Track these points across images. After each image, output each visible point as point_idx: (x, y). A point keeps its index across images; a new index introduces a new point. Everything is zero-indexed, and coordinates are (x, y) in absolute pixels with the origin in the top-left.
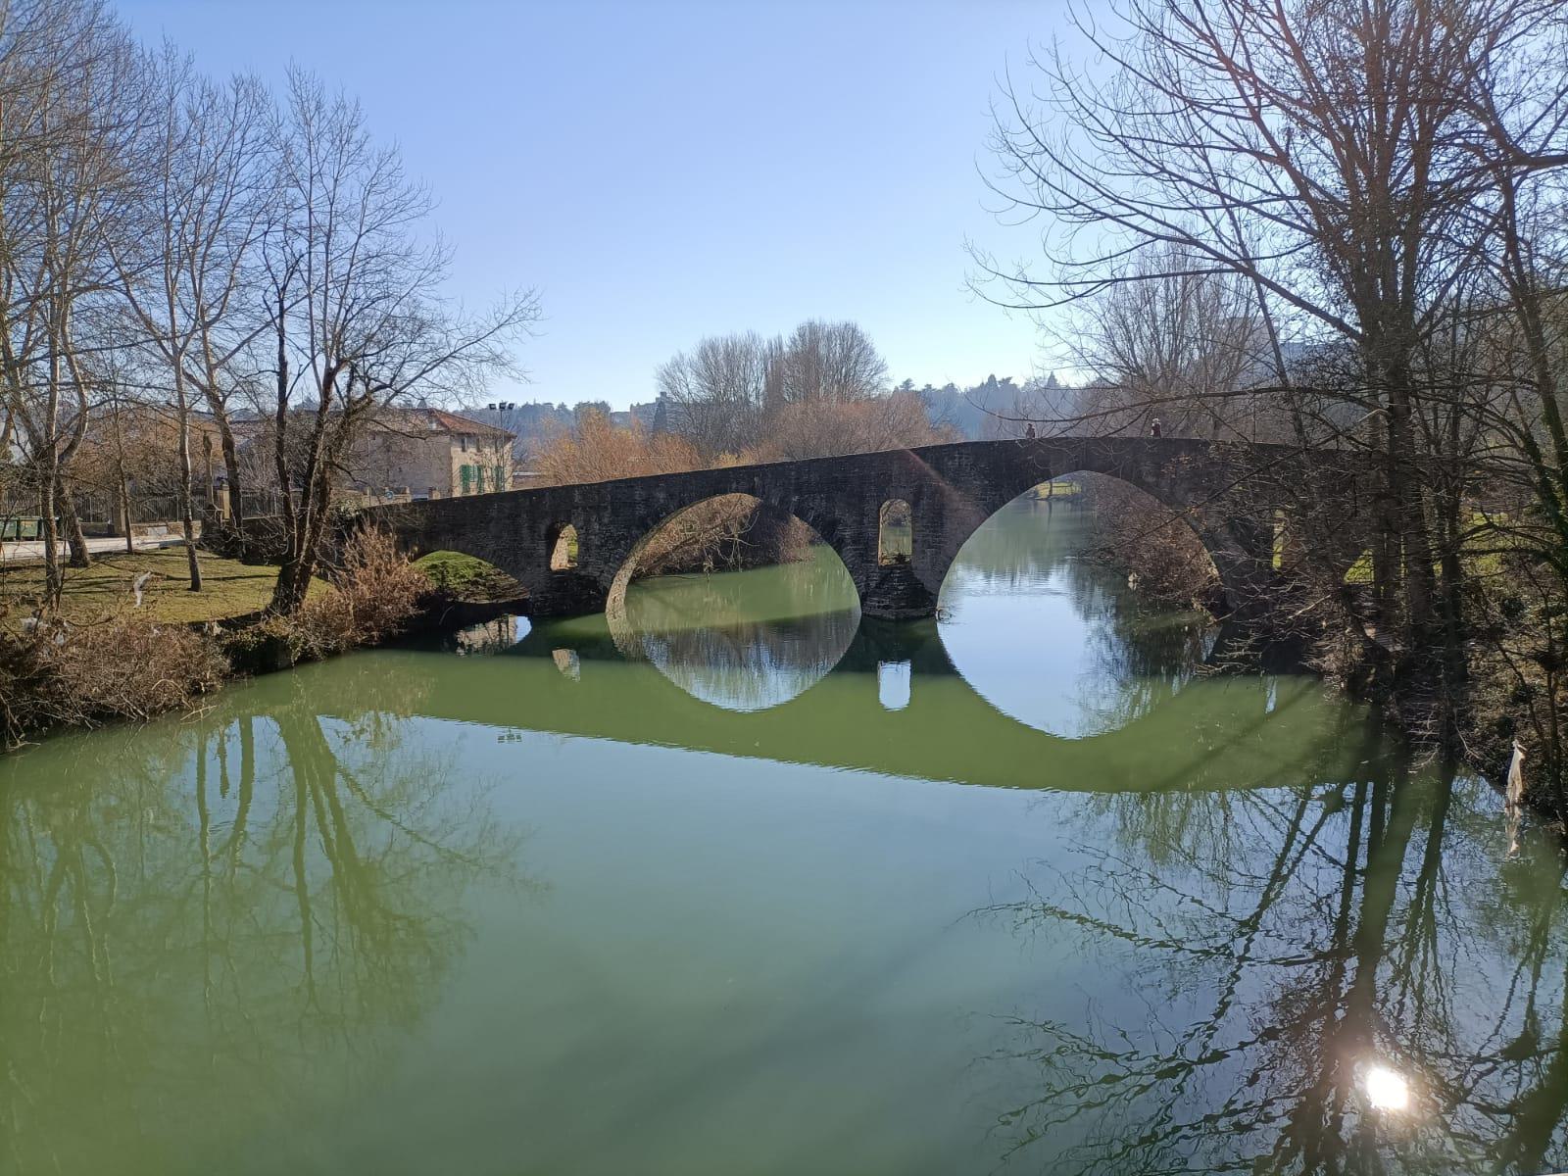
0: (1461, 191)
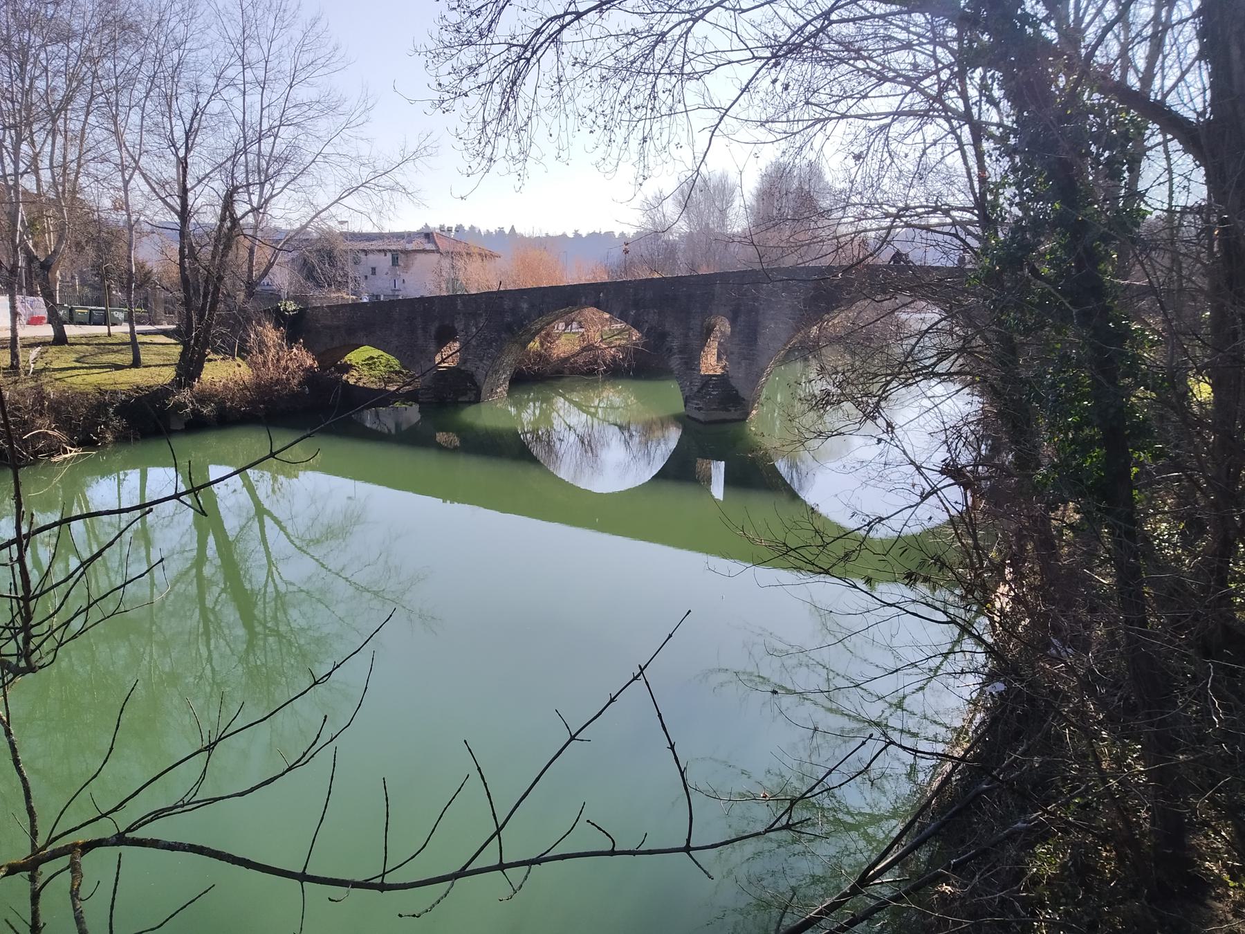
0: (230, 229)
